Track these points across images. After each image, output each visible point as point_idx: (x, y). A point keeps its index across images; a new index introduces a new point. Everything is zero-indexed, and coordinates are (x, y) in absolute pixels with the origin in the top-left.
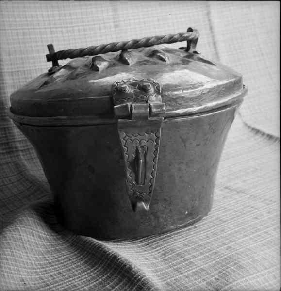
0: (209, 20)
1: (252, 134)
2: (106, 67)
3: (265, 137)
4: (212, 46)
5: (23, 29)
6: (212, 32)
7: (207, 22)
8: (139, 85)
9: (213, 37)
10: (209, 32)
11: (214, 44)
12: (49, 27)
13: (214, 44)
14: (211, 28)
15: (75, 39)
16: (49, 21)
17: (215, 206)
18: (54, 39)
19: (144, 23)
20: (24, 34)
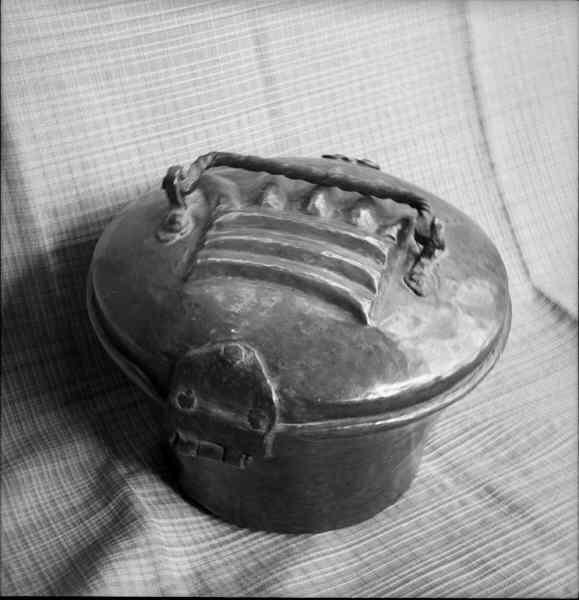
0: (471, 73)
1: (551, 319)
2: (427, 428)
3: (542, 300)
4: (476, 127)
5: (81, 157)
6: (476, 98)
7: (467, 77)
8: (181, 172)
9: (478, 107)
10: (469, 96)
11: (481, 122)
12: (111, 146)
13: (481, 122)
14: (475, 88)
15: (53, 155)
16: (110, 133)
17: (416, 493)
18: (146, 163)
19: (333, 97)
20: (84, 166)
